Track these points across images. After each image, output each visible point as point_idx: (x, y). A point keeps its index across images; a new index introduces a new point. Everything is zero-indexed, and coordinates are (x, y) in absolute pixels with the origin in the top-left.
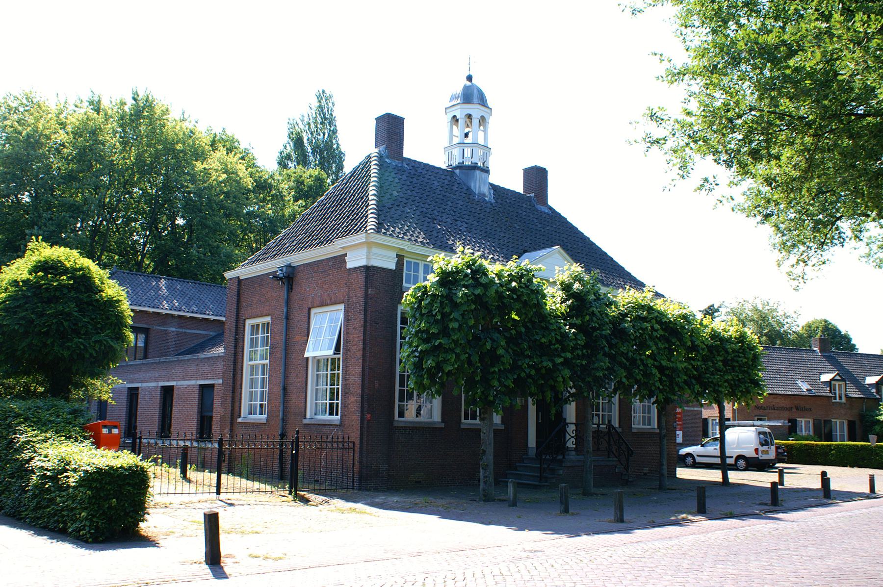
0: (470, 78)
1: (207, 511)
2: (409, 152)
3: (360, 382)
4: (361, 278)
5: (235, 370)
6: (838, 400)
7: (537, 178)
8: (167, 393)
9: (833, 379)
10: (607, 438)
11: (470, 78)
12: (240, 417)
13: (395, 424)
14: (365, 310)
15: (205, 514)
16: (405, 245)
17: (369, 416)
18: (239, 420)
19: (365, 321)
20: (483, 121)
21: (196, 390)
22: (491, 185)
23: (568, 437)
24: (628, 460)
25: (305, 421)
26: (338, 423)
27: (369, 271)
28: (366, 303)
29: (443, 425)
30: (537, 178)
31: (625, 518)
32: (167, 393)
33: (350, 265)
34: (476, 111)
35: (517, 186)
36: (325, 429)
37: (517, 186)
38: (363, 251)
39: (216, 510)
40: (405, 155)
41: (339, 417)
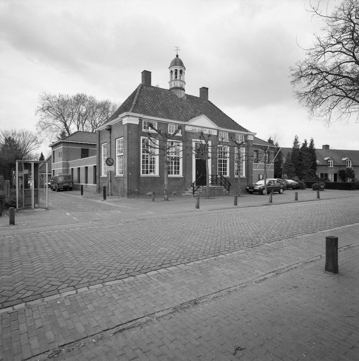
0: (177, 56)
1: (328, 235)
2: (153, 84)
3: (127, 163)
4: (126, 128)
5: (99, 161)
6: (330, 166)
7: (204, 91)
8: (87, 168)
9: (347, 160)
10: (220, 180)
11: (177, 56)
12: (101, 175)
13: (141, 176)
14: (128, 139)
15: (327, 238)
16: (141, 115)
17: (130, 174)
18: (101, 177)
19: (128, 142)
20: (181, 72)
21: (84, 168)
22: (185, 94)
23: (211, 180)
24: (229, 188)
25: (115, 176)
26: (123, 176)
27: (129, 125)
28: (128, 136)
29: (159, 176)
30: (204, 91)
31: (169, 199)
32: (87, 168)
33: (124, 123)
34: (179, 68)
35: (197, 94)
36: (120, 178)
37: (197, 94)
38: (127, 118)
39: (336, 236)
40: (152, 85)
41: (123, 175)
